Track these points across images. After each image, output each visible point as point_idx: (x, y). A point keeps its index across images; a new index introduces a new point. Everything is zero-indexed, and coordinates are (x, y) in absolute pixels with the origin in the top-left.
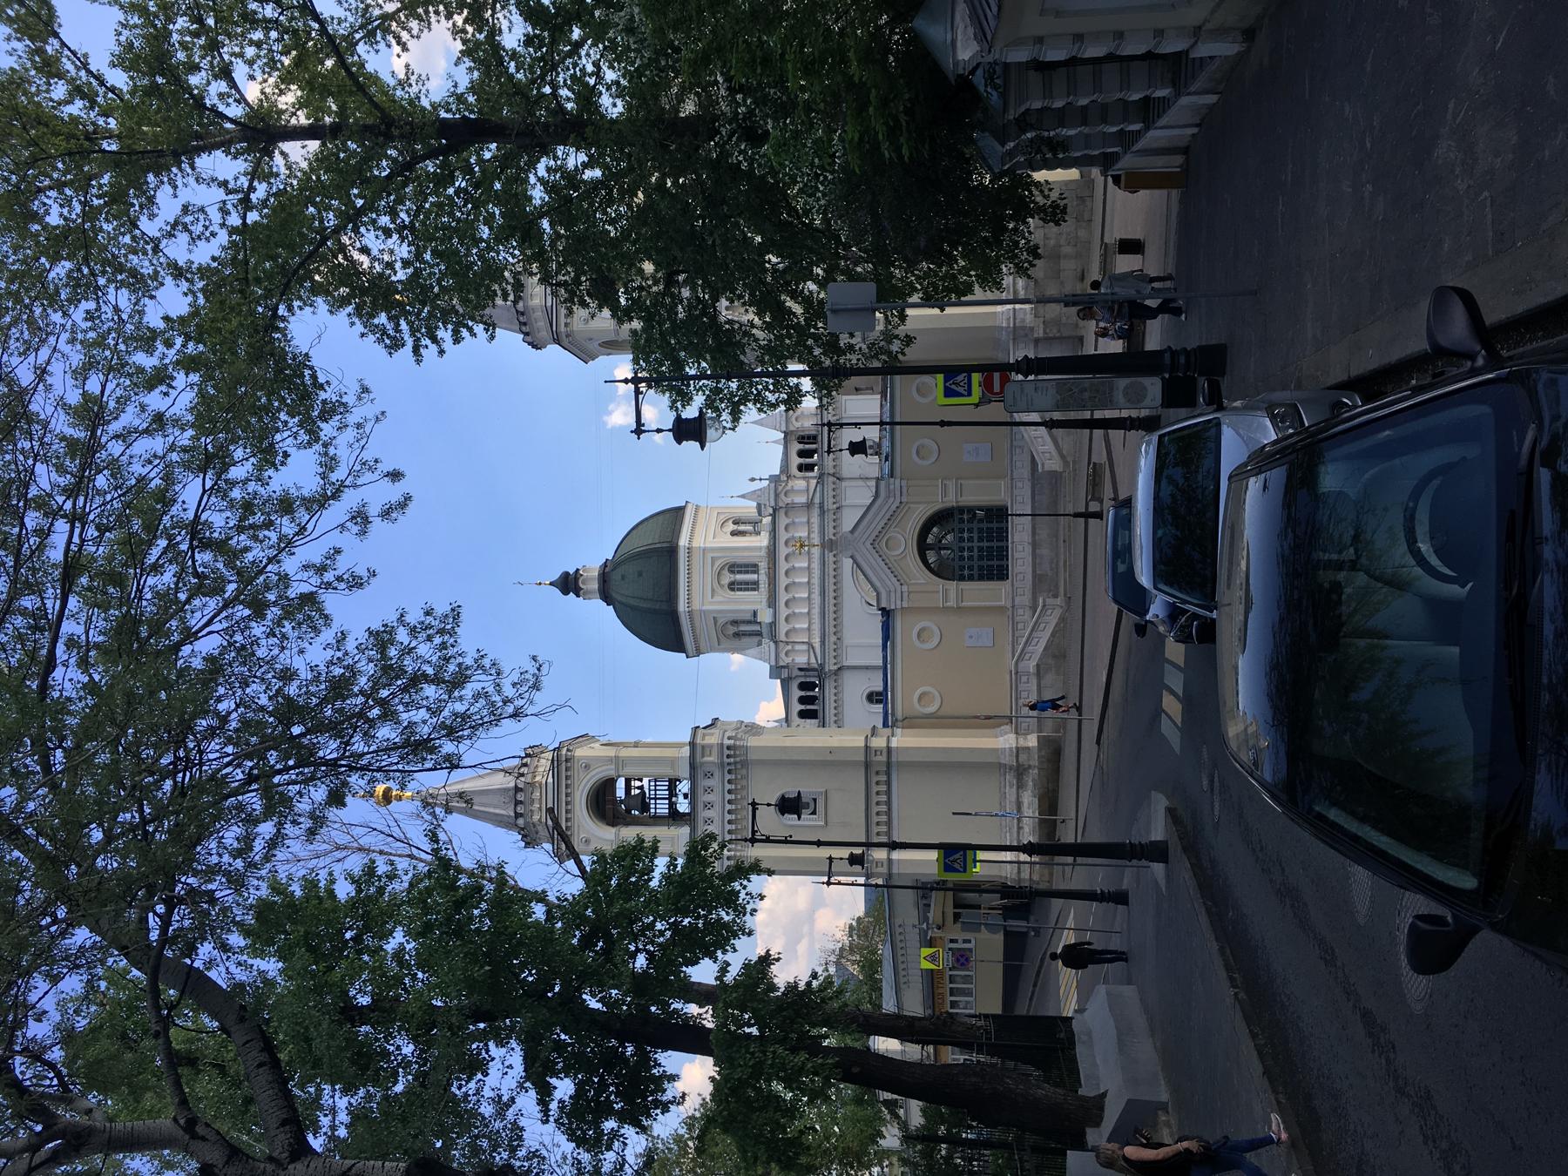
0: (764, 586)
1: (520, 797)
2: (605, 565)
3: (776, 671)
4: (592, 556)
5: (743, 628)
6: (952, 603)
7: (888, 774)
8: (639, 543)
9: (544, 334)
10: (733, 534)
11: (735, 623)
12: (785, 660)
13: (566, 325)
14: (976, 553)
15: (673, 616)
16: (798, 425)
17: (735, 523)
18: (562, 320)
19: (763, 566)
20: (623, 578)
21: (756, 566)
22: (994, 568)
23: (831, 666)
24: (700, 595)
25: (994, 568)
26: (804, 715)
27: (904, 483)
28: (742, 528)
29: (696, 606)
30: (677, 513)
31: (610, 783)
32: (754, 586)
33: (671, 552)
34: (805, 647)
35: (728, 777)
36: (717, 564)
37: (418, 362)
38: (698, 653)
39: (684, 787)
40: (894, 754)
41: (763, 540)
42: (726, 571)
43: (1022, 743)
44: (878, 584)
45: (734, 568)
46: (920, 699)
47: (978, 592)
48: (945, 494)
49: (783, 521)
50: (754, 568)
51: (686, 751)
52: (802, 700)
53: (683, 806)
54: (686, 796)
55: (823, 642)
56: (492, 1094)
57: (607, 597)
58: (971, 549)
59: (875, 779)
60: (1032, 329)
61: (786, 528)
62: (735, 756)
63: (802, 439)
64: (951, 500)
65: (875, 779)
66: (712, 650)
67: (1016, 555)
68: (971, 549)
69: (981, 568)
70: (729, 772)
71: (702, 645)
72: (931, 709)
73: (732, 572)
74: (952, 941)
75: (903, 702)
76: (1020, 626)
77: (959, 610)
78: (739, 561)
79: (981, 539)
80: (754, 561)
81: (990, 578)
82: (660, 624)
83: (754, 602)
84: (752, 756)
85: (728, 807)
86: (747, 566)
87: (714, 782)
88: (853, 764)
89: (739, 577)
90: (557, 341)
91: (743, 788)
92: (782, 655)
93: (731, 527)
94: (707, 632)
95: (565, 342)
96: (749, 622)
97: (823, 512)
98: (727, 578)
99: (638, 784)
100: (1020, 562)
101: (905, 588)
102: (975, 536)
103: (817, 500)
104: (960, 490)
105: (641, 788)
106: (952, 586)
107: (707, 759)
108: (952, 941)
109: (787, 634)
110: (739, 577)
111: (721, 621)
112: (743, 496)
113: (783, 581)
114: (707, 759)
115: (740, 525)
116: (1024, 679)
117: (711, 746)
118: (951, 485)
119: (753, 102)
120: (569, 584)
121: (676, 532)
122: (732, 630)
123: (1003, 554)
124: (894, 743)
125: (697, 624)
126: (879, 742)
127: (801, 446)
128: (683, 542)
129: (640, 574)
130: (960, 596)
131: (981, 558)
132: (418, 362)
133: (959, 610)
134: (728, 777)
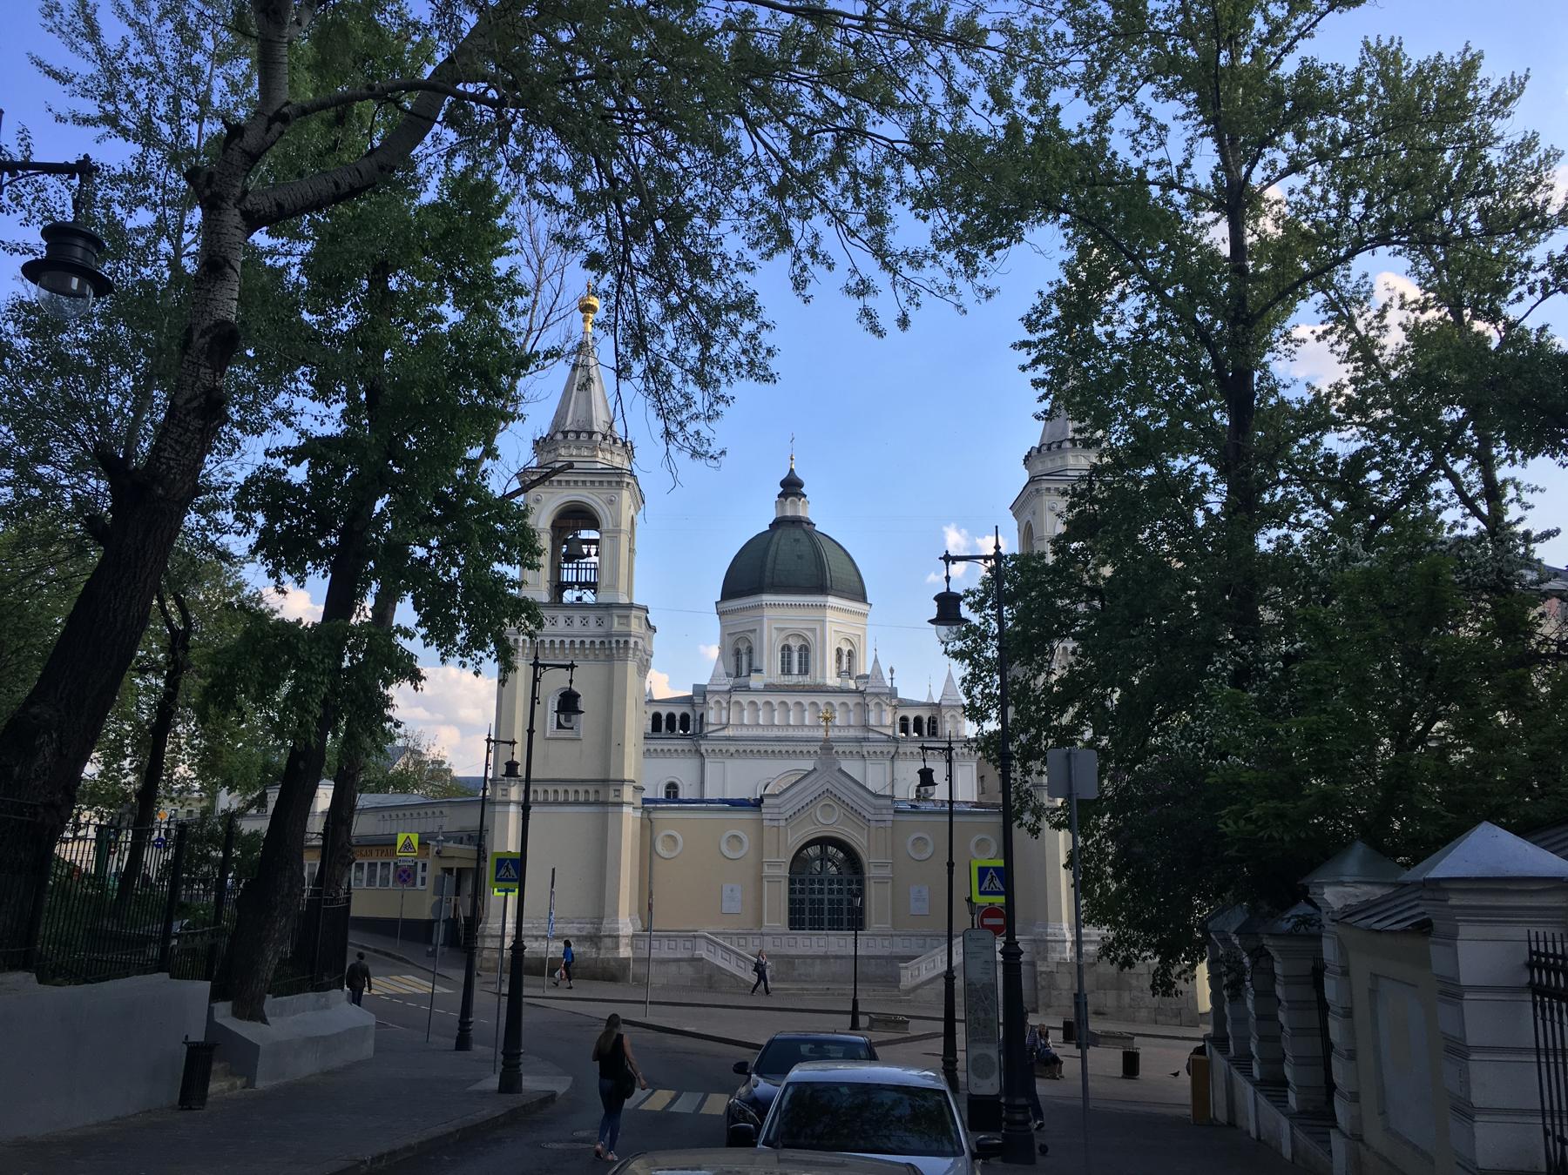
1: (584, 436)
2: (810, 523)
3: (701, 691)
4: (818, 510)
6: (767, 871)
7: (596, 803)
9: (1042, 466)
10: (839, 651)
11: (750, 651)
12: (711, 700)
13: (1048, 489)
14: (817, 896)
16: (947, 717)
17: (850, 653)
18: (1052, 486)
19: (807, 680)
20: (797, 540)
21: (806, 672)
22: (802, 915)
23: (705, 746)
24: (778, 615)
25: (802, 915)
26: (656, 718)
27: (889, 824)
28: (845, 659)
30: (861, 596)
31: (594, 524)
32: (786, 670)
33: (821, 588)
34: (724, 720)
35: (597, 641)
38: (721, 614)
39: (588, 597)
40: (616, 809)
41: (832, 680)
43: (623, 941)
44: (788, 795)
45: (805, 650)
47: (777, 899)
49: (851, 701)
50: (804, 670)
51: (624, 600)
52: (671, 717)
53: (569, 596)
54: (579, 599)
55: (728, 739)
57: (776, 524)
58: (821, 891)
59: (591, 789)
60: (1045, 959)
61: (844, 704)
62: (618, 648)
63: (933, 722)
64: (871, 872)
65: (591, 789)
66: (723, 627)
67: (814, 939)
68: (821, 891)
69: (802, 902)
70: (602, 643)
71: (729, 617)
72: (659, 848)
74: (424, 865)
75: (668, 819)
76: (742, 942)
77: (760, 879)
78: (812, 655)
79: (831, 902)
81: (791, 911)
82: (750, 576)
83: (770, 669)
84: (617, 664)
85: (567, 641)
86: (807, 663)
87: (592, 627)
88: (607, 768)
89: (795, 656)
90: (1032, 480)
91: (586, 656)
92: (717, 698)
93: (846, 648)
94: (742, 622)
95: (1032, 488)
96: (750, 665)
97: (858, 740)
98: (795, 644)
99: (593, 551)
100: (807, 942)
101: (782, 823)
102: (835, 896)
103: (871, 735)
104: (881, 881)
105: (589, 555)
106: (784, 872)
107: (616, 620)
108: (424, 865)
109: (738, 703)
110: (795, 656)
111: (751, 636)
112: (876, 661)
113: (791, 699)
114: (616, 620)
115: (846, 658)
116: (688, 944)
117: (629, 625)
118: (887, 872)
120: (791, 487)
121: (841, 594)
122: (743, 648)
123: (817, 925)
124: (627, 810)
126: (628, 794)
127: (926, 720)
128: (832, 601)
129: (800, 557)
130: (773, 880)
131: (812, 902)
133: (760, 879)
134: (597, 641)
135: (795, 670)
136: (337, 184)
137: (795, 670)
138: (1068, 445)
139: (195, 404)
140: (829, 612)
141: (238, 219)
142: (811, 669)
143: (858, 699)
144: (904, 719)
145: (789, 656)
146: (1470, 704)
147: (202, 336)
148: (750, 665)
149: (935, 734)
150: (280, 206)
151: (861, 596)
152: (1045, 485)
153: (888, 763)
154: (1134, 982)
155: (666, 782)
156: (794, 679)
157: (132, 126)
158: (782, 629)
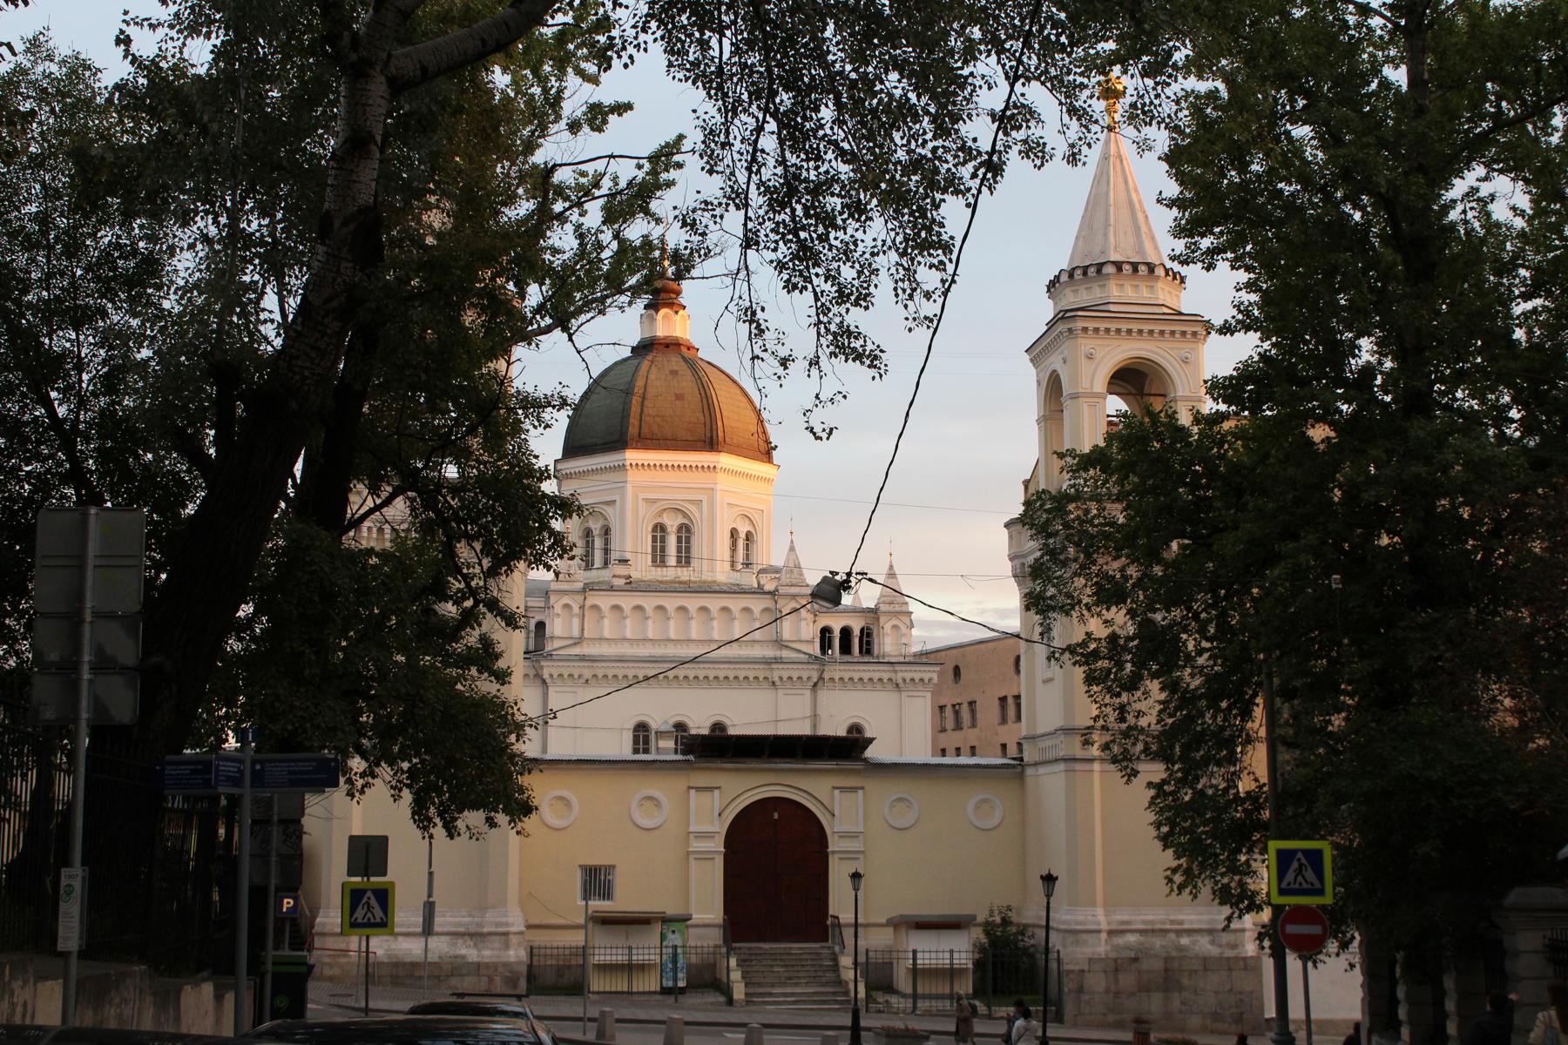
0: (735, 578)
5: (598, 543)
8: (724, 397)
9: (1071, 299)
10: (734, 533)
11: (606, 531)
13: (1085, 329)
15: (618, 442)
16: (888, 628)
17: (749, 536)
18: (1091, 325)
19: (684, 574)
20: (674, 373)
21: (688, 563)
23: (548, 669)
28: (741, 543)
29: (633, 477)
30: (766, 452)
32: (659, 558)
33: (711, 443)
34: (576, 633)
36: (692, 508)
37: (628, 107)
41: (722, 573)
42: (680, 520)
45: (685, 532)
46: (561, 798)
48: (844, 835)
49: (757, 605)
50: (685, 559)
56: (1151, 131)
61: (746, 610)
63: (866, 634)
73: (680, 528)
80: (694, 563)
86: (688, 549)
89: (672, 541)
90: (1062, 317)
92: (566, 600)
93: (743, 529)
95: (1061, 327)
96: (606, 551)
97: (768, 662)
98: (672, 523)
103: (785, 654)
106: (718, 845)
109: (595, 607)
110: (672, 541)
111: (609, 510)
112: (792, 549)
113: (671, 602)
115: (743, 542)
119: (386, 575)
125: (604, 477)
127: (857, 632)
128: (725, 460)
129: (679, 397)
130: (704, 857)
132: (628, 107)
135: (672, 561)
136: (483, 41)
137: (672, 561)
138: (1110, 269)
139: (335, 304)
140: (720, 476)
141: (384, 87)
142: (695, 552)
143: (767, 602)
144: (826, 631)
145: (663, 540)
146: (207, 181)
147: (344, 224)
148: (606, 551)
149: (869, 652)
150: (424, 69)
151: (766, 452)
152: (1080, 324)
153: (808, 693)
154: (1186, 982)
155: (631, 724)
156: (671, 573)
157: (799, 208)
158: (654, 501)
